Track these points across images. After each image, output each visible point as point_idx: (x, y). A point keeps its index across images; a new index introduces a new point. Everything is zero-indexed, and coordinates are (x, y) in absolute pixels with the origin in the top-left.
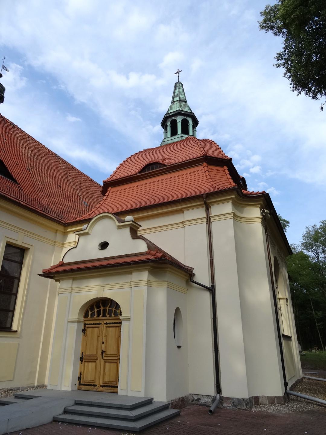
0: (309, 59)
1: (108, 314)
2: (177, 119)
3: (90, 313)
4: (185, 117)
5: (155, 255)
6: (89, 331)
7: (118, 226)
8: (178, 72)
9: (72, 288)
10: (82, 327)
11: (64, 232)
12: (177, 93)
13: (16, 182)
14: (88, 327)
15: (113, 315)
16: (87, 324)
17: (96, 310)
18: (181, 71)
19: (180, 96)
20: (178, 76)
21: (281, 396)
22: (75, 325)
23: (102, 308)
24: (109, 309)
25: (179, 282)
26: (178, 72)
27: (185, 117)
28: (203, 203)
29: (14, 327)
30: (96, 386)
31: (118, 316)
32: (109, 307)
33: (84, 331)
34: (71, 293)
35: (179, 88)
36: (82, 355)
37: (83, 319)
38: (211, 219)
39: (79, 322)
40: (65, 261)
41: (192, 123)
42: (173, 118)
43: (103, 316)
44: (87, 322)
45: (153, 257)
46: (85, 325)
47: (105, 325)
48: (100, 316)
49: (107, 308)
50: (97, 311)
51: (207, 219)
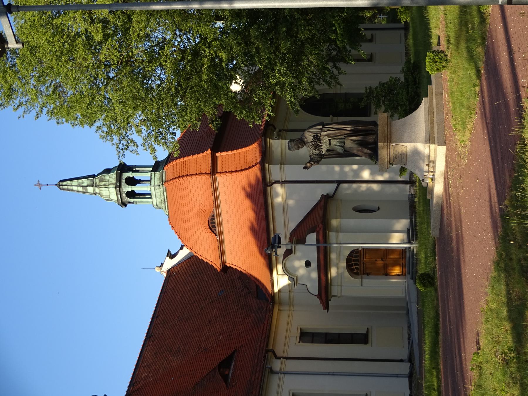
0: (519, 354)
1: (357, 258)
2: (126, 191)
3: (356, 271)
4: (123, 181)
5: (321, 228)
6: (368, 271)
7: (295, 254)
8: (39, 185)
9: (338, 286)
10: (366, 276)
11: (279, 304)
12: (80, 189)
13: (233, 354)
14: (366, 272)
15: (358, 254)
16: (364, 272)
17: (354, 267)
18: (39, 181)
19: (86, 185)
20: (46, 186)
21: (367, 280)
22: (365, 281)
23: (353, 262)
24: (354, 258)
25: (332, 208)
26: (39, 185)
27: (123, 181)
28: (269, 188)
29: (364, 332)
30: (402, 263)
31: (358, 251)
32: (352, 257)
33: (368, 274)
34: (342, 286)
35: (72, 186)
36: (384, 274)
37: (360, 276)
38: (283, 180)
39: (362, 279)
40: (316, 292)
41: (131, 173)
42: (124, 195)
43: (358, 262)
44: (362, 273)
45: (322, 230)
46: (364, 274)
47: (365, 260)
48: (358, 263)
49: (353, 259)
50: (355, 266)
51: (283, 183)
